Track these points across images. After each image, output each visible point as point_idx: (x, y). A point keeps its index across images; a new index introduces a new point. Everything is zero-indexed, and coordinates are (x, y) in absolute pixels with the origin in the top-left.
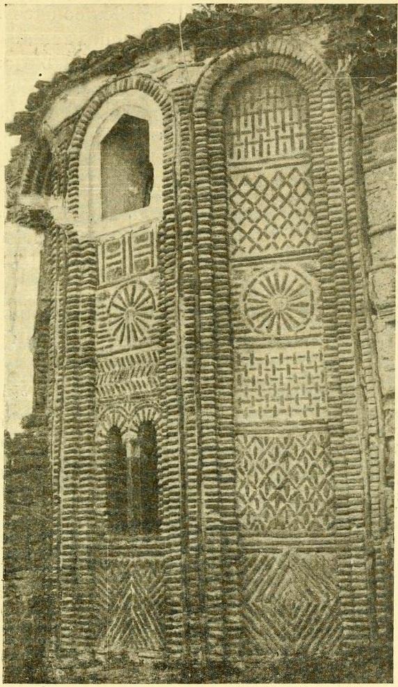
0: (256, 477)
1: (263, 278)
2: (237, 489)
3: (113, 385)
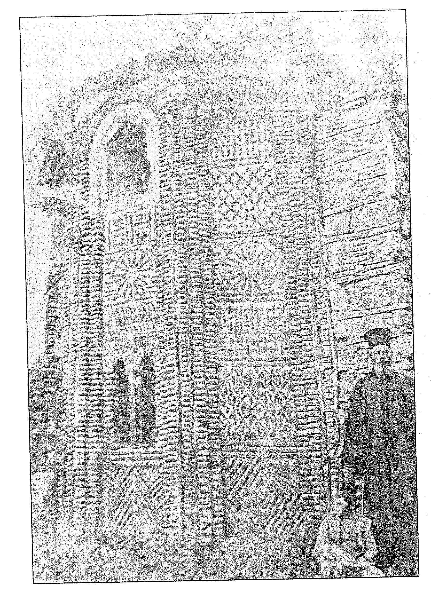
0: (234, 399)
1: (237, 249)
2: (220, 408)
3: (118, 328)
